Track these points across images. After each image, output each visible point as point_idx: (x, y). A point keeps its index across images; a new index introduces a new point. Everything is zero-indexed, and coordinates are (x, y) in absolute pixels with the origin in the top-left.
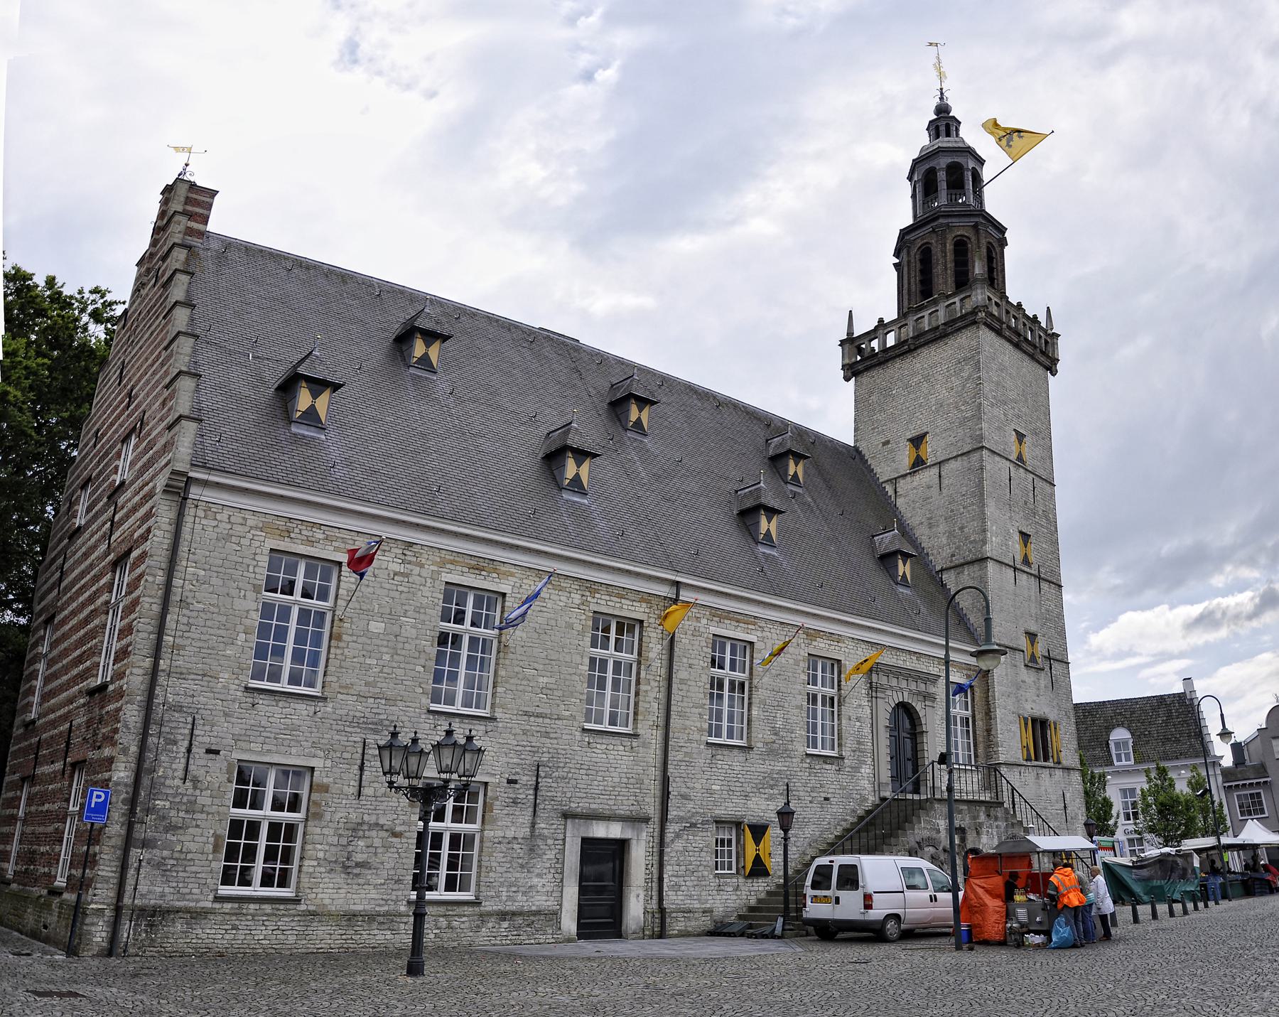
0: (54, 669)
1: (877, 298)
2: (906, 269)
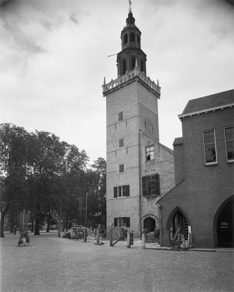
0: (68, 223)
1: (112, 73)
2: (119, 66)
